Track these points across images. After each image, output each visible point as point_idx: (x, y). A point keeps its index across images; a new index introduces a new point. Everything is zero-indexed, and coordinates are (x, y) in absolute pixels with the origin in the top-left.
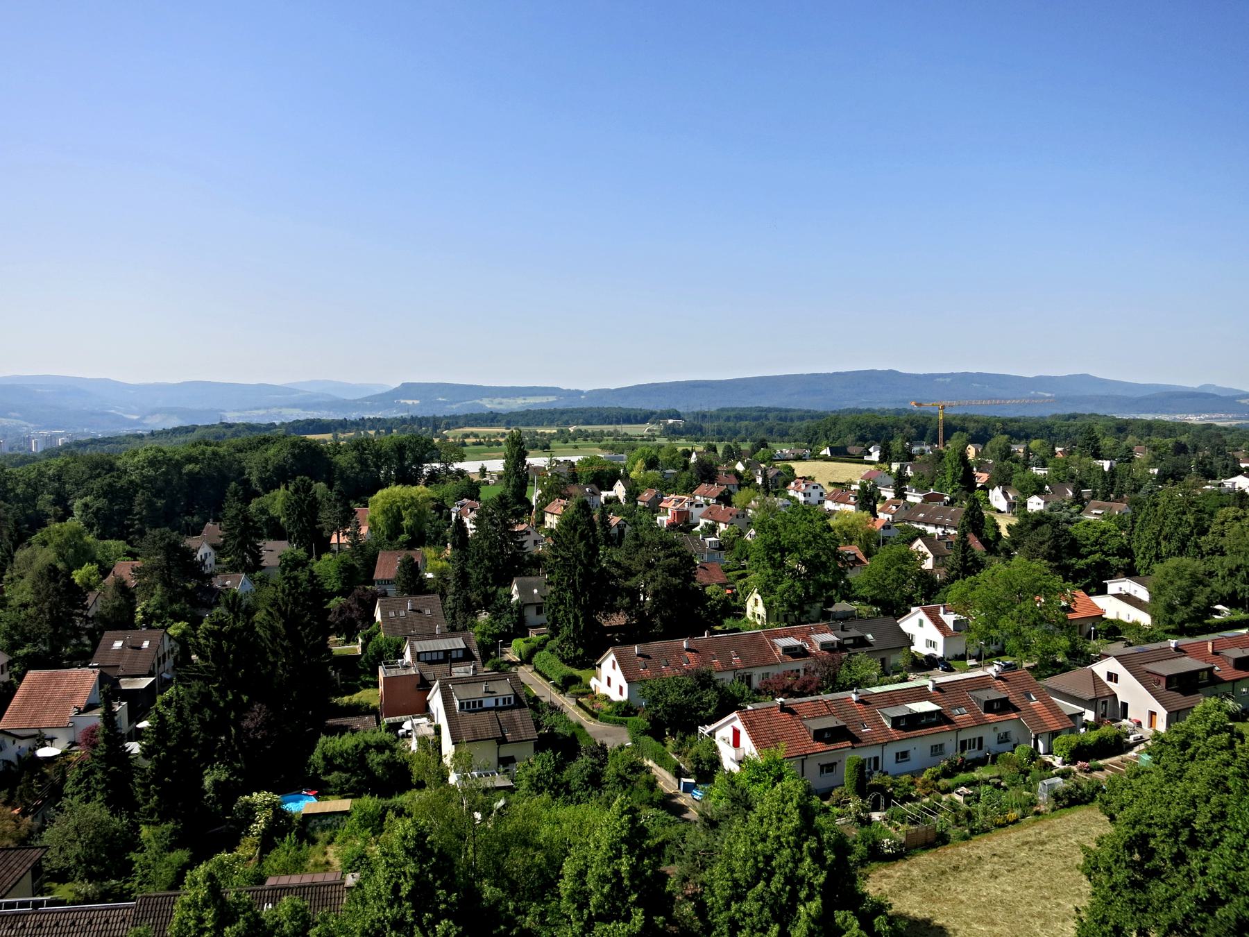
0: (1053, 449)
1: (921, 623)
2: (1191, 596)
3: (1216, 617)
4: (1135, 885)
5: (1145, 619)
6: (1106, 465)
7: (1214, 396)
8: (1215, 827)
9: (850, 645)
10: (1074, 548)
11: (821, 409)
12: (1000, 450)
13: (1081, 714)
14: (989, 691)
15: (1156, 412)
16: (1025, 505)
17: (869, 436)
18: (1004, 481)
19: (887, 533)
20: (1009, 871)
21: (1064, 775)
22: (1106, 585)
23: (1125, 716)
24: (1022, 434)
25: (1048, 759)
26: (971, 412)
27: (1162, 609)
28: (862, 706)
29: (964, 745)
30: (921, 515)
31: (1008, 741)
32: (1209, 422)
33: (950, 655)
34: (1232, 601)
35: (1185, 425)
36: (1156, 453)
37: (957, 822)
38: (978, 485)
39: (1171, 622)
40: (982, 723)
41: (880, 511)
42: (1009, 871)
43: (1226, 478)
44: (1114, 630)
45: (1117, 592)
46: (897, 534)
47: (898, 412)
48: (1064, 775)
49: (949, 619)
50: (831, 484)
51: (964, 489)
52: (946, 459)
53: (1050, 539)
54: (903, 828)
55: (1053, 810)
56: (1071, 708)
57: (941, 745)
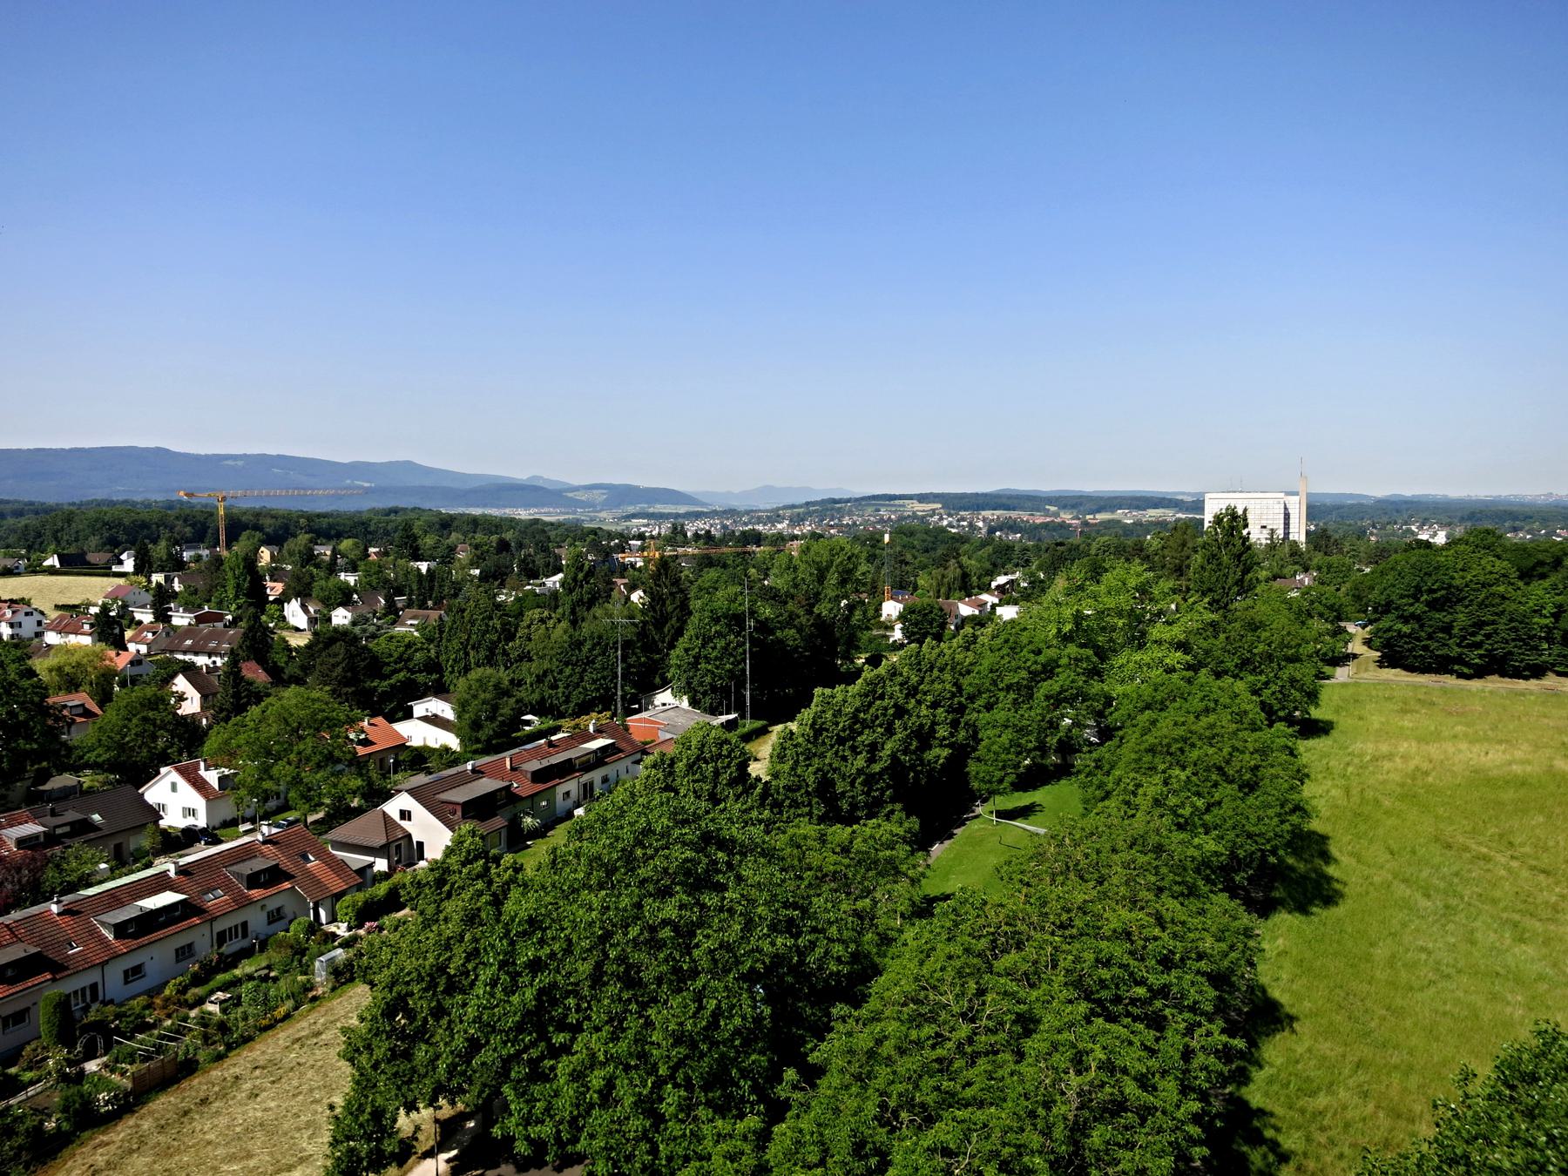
0: (366, 550)
1: (174, 787)
2: (495, 708)
3: (527, 728)
4: (394, 1055)
5: (453, 742)
6: (423, 567)
7: (542, 488)
8: (470, 966)
9: (65, 835)
10: (376, 666)
11: (51, 500)
12: (300, 552)
13: (371, 865)
14: (254, 861)
15: (485, 506)
16: (329, 620)
17: (122, 537)
18: (301, 590)
19: (137, 670)
20: (273, 1082)
21: (347, 944)
22: (411, 707)
23: (421, 857)
24: (333, 532)
25: (332, 928)
26: (271, 505)
27: (469, 728)
28: (67, 918)
29: (222, 938)
30: (189, 642)
31: (282, 918)
32: (537, 517)
33: (217, 823)
34: (541, 709)
35: (512, 520)
36: (479, 552)
37: (206, 1038)
38: (271, 598)
39: (478, 741)
40: (243, 903)
41: (130, 641)
42: (273, 1082)
43: (548, 577)
44: (418, 759)
45: (424, 714)
46: (152, 670)
47: (170, 505)
48: (347, 944)
49: (212, 777)
50: (57, 607)
51: (250, 604)
52: (226, 567)
53: (344, 659)
54: (131, 1069)
55: (333, 989)
56: (357, 860)
57: (190, 946)
